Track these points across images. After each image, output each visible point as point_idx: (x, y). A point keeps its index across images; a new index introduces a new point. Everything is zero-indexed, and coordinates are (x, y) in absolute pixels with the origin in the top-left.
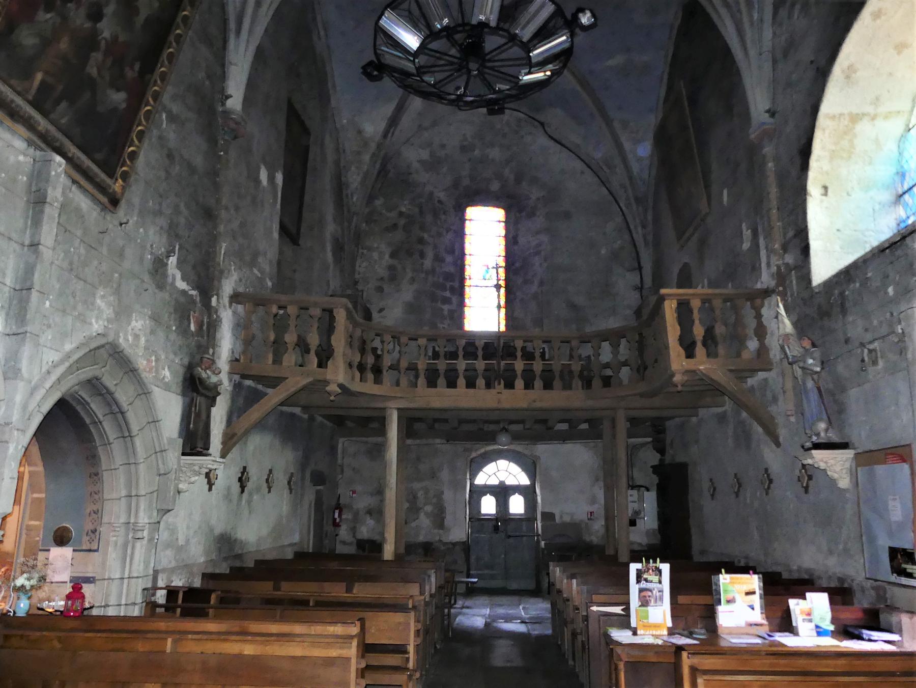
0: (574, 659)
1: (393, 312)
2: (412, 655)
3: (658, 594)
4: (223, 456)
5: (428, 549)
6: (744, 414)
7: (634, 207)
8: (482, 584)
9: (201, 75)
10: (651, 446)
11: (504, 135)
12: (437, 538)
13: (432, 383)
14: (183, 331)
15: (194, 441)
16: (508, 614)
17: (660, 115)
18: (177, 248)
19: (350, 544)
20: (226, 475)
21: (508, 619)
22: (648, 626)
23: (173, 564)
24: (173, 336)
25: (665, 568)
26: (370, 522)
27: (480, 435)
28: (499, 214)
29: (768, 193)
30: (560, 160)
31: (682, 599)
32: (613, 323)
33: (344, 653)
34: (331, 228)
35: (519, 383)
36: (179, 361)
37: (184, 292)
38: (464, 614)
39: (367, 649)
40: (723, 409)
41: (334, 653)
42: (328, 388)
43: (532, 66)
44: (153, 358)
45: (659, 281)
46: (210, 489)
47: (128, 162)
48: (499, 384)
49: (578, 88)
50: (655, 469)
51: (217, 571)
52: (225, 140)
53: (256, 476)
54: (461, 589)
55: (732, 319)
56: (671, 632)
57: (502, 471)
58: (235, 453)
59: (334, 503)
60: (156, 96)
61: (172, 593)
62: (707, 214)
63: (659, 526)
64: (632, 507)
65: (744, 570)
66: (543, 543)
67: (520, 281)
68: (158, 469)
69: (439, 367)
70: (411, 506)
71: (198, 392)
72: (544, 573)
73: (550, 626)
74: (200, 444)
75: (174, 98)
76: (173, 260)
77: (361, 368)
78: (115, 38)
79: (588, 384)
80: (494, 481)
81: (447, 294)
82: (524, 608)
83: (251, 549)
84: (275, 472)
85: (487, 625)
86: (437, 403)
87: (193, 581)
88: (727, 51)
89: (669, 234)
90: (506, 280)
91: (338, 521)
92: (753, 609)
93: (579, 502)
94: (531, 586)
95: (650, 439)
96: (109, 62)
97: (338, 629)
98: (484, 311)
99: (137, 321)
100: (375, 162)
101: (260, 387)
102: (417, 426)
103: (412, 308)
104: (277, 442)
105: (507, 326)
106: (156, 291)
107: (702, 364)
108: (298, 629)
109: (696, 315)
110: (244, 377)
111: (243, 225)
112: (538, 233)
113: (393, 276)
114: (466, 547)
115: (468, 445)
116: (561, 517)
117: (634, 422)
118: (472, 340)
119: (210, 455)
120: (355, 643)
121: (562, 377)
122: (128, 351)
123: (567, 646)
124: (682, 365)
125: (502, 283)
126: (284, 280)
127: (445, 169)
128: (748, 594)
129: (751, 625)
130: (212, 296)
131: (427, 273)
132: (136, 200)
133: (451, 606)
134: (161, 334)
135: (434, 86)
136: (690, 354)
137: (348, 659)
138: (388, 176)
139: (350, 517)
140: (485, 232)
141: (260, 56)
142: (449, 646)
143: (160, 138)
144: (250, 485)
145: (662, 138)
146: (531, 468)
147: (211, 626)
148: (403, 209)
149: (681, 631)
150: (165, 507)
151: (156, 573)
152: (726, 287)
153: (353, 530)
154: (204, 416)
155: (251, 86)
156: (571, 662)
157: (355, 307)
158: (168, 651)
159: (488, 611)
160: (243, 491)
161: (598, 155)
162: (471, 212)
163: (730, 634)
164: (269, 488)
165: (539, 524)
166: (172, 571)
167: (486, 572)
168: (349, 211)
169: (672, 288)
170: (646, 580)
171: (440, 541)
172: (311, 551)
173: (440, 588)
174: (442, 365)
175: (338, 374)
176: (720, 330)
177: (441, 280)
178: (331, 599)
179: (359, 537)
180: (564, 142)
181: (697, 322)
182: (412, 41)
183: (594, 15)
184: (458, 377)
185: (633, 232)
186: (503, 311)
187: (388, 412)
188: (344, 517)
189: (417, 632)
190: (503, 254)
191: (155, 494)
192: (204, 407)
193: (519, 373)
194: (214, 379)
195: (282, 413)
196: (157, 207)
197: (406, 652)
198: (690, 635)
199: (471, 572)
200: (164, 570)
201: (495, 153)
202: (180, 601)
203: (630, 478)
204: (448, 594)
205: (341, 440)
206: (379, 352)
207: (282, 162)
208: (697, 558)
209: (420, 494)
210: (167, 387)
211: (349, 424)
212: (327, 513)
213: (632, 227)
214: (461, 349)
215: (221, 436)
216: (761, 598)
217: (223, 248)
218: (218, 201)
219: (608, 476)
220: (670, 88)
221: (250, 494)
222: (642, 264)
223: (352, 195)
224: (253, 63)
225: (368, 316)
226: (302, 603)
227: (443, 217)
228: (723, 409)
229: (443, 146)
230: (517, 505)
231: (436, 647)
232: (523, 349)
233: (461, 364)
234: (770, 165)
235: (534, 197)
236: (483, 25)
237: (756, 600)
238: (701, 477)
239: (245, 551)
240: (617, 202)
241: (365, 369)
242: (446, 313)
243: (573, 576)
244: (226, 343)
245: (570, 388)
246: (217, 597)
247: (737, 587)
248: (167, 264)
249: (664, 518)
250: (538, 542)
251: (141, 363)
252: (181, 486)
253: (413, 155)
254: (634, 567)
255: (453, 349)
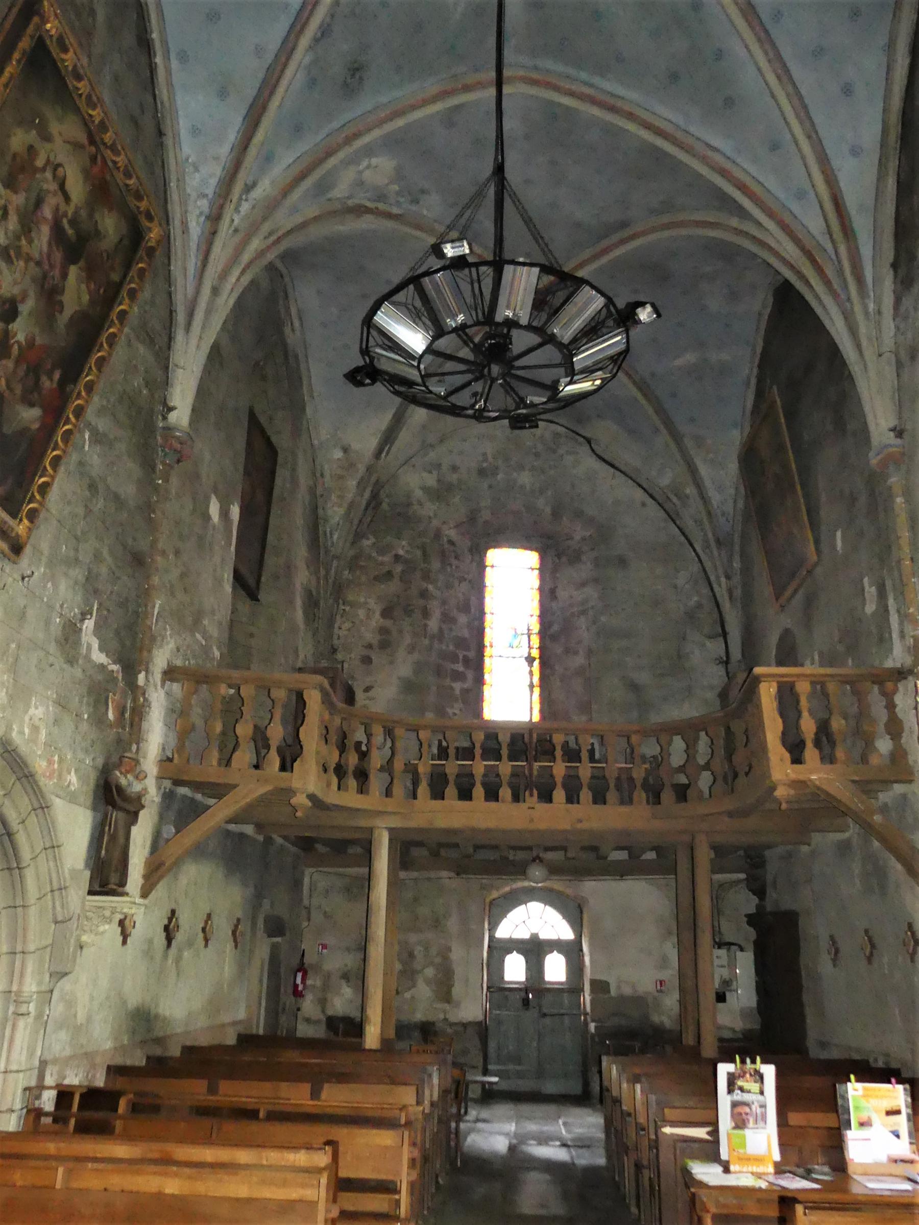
0: (638, 1206)
1: (382, 693)
2: (404, 1197)
3: (759, 1111)
4: (144, 895)
5: (427, 1031)
6: (876, 844)
7: (716, 553)
8: (505, 1086)
9: (138, 381)
10: (743, 885)
11: (537, 455)
12: (442, 1016)
13: (438, 794)
14: (99, 721)
15: (106, 876)
16: (542, 1132)
17: (747, 429)
18: (95, 608)
19: (318, 1022)
20: (146, 917)
21: (543, 1140)
22: (747, 1159)
23: (68, 1052)
24: (84, 727)
25: (769, 1071)
26: (347, 991)
27: (502, 866)
28: (531, 558)
29: (898, 538)
30: (614, 489)
31: (795, 1118)
32: (687, 711)
33: (309, 1194)
34: (302, 577)
35: (559, 795)
36: (91, 762)
37: (102, 667)
38: (479, 1131)
39: (343, 1185)
40: (847, 835)
41: (294, 1194)
42: (294, 801)
43: (572, 374)
44: (56, 758)
45: (751, 657)
46: (124, 942)
47: (38, 497)
48: (531, 795)
49: (639, 396)
50: (752, 920)
51: (129, 1062)
52: (164, 463)
53: (189, 922)
54: (474, 1092)
55: (855, 709)
56: (779, 1170)
57: (534, 920)
58: (160, 891)
59: (295, 962)
60: (79, 412)
61: (64, 1096)
62: (816, 564)
63: (759, 1003)
64: (720, 973)
65: (884, 1075)
66: (592, 1027)
67: (558, 649)
68: (54, 915)
69: (447, 771)
70: (405, 971)
71: (115, 806)
72: (595, 1069)
73: (602, 1151)
74: (114, 878)
75: (101, 411)
76: (89, 625)
77: (340, 771)
78: (31, 343)
79: (655, 797)
80: (523, 934)
81: (460, 667)
82: (565, 1124)
83: (179, 1031)
84: (215, 918)
85: (512, 1148)
86: (441, 823)
87: (94, 1076)
88: (835, 352)
89: (764, 588)
90: (540, 648)
91: (300, 988)
92: (898, 1136)
93: (644, 969)
94: (575, 1088)
95: (742, 876)
96: (21, 372)
97: (301, 1158)
98: (510, 694)
99: (36, 708)
100: (365, 489)
101: (199, 797)
102: (416, 852)
103: (409, 687)
104: (220, 874)
105: (542, 711)
106: (65, 666)
107: (815, 772)
108: (243, 1156)
109: (804, 703)
110: (177, 783)
111: (183, 575)
112: (583, 584)
113: (386, 643)
114: (482, 1030)
115: (485, 880)
116: (619, 987)
117: (719, 851)
118: (493, 732)
119: (127, 894)
120: (324, 1180)
121: (618, 788)
122: (23, 749)
123: (629, 1186)
124: (787, 775)
125: (535, 653)
126: (237, 649)
127: (457, 499)
128: (889, 1113)
129: (896, 1161)
130: (140, 672)
131: (433, 637)
132: (45, 546)
133: (459, 1118)
134: (68, 722)
135: (445, 398)
136: (797, 760)
137: (313, 1204)
138: (380, 509)
139: (318, 983)
140: (512, 583)
141: (215, 354)
142: (453, 1172)
143: (81, 464)
144: (180, 937)
145: (749, 458)
146: (575, 912)
147: (121, 1150)
148: (401, 552)
149: (794, 1169)
150: (60, 969)
151: (43, 1064)
152: (843, 664)
153: (323, 1002)
154: (122, 840)
155: (202, 393)
156: (634, 1210)
157: (332, 685)
158: (58, 1186)
159: (512, 1127)
160: (169, 944)
161: (665, 481)
162: (494, 556)
163: (865, 1174)
164: (206, 940)
165: (587, 997)
166: (66, 1062)
167: (511, 1067)
168: (327, 552)
169: (769, 665)
170: (741, 1089)
171: (446, 1019)
172: (261, 1032)
173: (444, 1092)
174: (452, 767)
175: (308, 780)
176: (837, 724)
177: (451, 647)
178: (289, 1109)
179: (330, 1012)
180: (617, 465)
181: (805, 714)
182: (415, 340)
183: (656, 310)
184: (473, 785)
185: (715, 586)
186: (537, 691)
187: (376, 833)
188: (309, 982)
189: (413, 1162)
190: (537, 612)
191: (49, 949)
192: (121, 823)
193: (559, 780)
194: (137, 787)
195: (228, 833)
196: (72, 554)
197: (397, 1191)
198: (807, 1175)
199: (490, 1067)
200: (55, 1061)
201: (525, 479)
202: (75, 1107)
203: (716, 931)
204: (457, 1095)
205: (308, 871)
206: (364, 748)
207: (239, 488)
208: (815, 1052)
209: (418, 951)
210: (72, 798)
211: (320, 848)
212: (286, 976)
213: (712, 578)
214: (478, 746)
215: (143, 865)
216: (909, 1120)
217: (157, 606)
218: (154, 544)
219: (687, 928)
220: (760, 394)
221: (180, 950)
222: (728, 629)
223: (331, 534)
224: (206, 366)
225: (350, 698)
226: (249, 1114)
227: (455, 562)
228: (847, 835)
229: (454, 468)
230: (555, 969)
231: (437, 1182)
232: (565, 745)
233: (479, 767)
234: (899, 500)
235: (577, 537)
236: (511, 324)
237: (902, 1122)
238: (817, 929)
239: (168, 1033)
240: (691, 545)
241: (345, 773)
242: (457, 692)
243: (636, 1079)
244: (156, 736)
245: (630, 802)
246: (129, 1101)
247: (874, 1102)
248: (81, 629)
249: (763, 989)
250: (586, 1024)
251: (40, 765)
252: (84, 938)
253: (414, 481)
254: (724, 1069)
255: (466, 744)
